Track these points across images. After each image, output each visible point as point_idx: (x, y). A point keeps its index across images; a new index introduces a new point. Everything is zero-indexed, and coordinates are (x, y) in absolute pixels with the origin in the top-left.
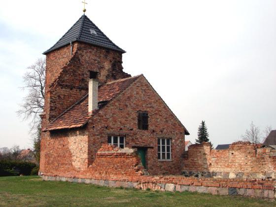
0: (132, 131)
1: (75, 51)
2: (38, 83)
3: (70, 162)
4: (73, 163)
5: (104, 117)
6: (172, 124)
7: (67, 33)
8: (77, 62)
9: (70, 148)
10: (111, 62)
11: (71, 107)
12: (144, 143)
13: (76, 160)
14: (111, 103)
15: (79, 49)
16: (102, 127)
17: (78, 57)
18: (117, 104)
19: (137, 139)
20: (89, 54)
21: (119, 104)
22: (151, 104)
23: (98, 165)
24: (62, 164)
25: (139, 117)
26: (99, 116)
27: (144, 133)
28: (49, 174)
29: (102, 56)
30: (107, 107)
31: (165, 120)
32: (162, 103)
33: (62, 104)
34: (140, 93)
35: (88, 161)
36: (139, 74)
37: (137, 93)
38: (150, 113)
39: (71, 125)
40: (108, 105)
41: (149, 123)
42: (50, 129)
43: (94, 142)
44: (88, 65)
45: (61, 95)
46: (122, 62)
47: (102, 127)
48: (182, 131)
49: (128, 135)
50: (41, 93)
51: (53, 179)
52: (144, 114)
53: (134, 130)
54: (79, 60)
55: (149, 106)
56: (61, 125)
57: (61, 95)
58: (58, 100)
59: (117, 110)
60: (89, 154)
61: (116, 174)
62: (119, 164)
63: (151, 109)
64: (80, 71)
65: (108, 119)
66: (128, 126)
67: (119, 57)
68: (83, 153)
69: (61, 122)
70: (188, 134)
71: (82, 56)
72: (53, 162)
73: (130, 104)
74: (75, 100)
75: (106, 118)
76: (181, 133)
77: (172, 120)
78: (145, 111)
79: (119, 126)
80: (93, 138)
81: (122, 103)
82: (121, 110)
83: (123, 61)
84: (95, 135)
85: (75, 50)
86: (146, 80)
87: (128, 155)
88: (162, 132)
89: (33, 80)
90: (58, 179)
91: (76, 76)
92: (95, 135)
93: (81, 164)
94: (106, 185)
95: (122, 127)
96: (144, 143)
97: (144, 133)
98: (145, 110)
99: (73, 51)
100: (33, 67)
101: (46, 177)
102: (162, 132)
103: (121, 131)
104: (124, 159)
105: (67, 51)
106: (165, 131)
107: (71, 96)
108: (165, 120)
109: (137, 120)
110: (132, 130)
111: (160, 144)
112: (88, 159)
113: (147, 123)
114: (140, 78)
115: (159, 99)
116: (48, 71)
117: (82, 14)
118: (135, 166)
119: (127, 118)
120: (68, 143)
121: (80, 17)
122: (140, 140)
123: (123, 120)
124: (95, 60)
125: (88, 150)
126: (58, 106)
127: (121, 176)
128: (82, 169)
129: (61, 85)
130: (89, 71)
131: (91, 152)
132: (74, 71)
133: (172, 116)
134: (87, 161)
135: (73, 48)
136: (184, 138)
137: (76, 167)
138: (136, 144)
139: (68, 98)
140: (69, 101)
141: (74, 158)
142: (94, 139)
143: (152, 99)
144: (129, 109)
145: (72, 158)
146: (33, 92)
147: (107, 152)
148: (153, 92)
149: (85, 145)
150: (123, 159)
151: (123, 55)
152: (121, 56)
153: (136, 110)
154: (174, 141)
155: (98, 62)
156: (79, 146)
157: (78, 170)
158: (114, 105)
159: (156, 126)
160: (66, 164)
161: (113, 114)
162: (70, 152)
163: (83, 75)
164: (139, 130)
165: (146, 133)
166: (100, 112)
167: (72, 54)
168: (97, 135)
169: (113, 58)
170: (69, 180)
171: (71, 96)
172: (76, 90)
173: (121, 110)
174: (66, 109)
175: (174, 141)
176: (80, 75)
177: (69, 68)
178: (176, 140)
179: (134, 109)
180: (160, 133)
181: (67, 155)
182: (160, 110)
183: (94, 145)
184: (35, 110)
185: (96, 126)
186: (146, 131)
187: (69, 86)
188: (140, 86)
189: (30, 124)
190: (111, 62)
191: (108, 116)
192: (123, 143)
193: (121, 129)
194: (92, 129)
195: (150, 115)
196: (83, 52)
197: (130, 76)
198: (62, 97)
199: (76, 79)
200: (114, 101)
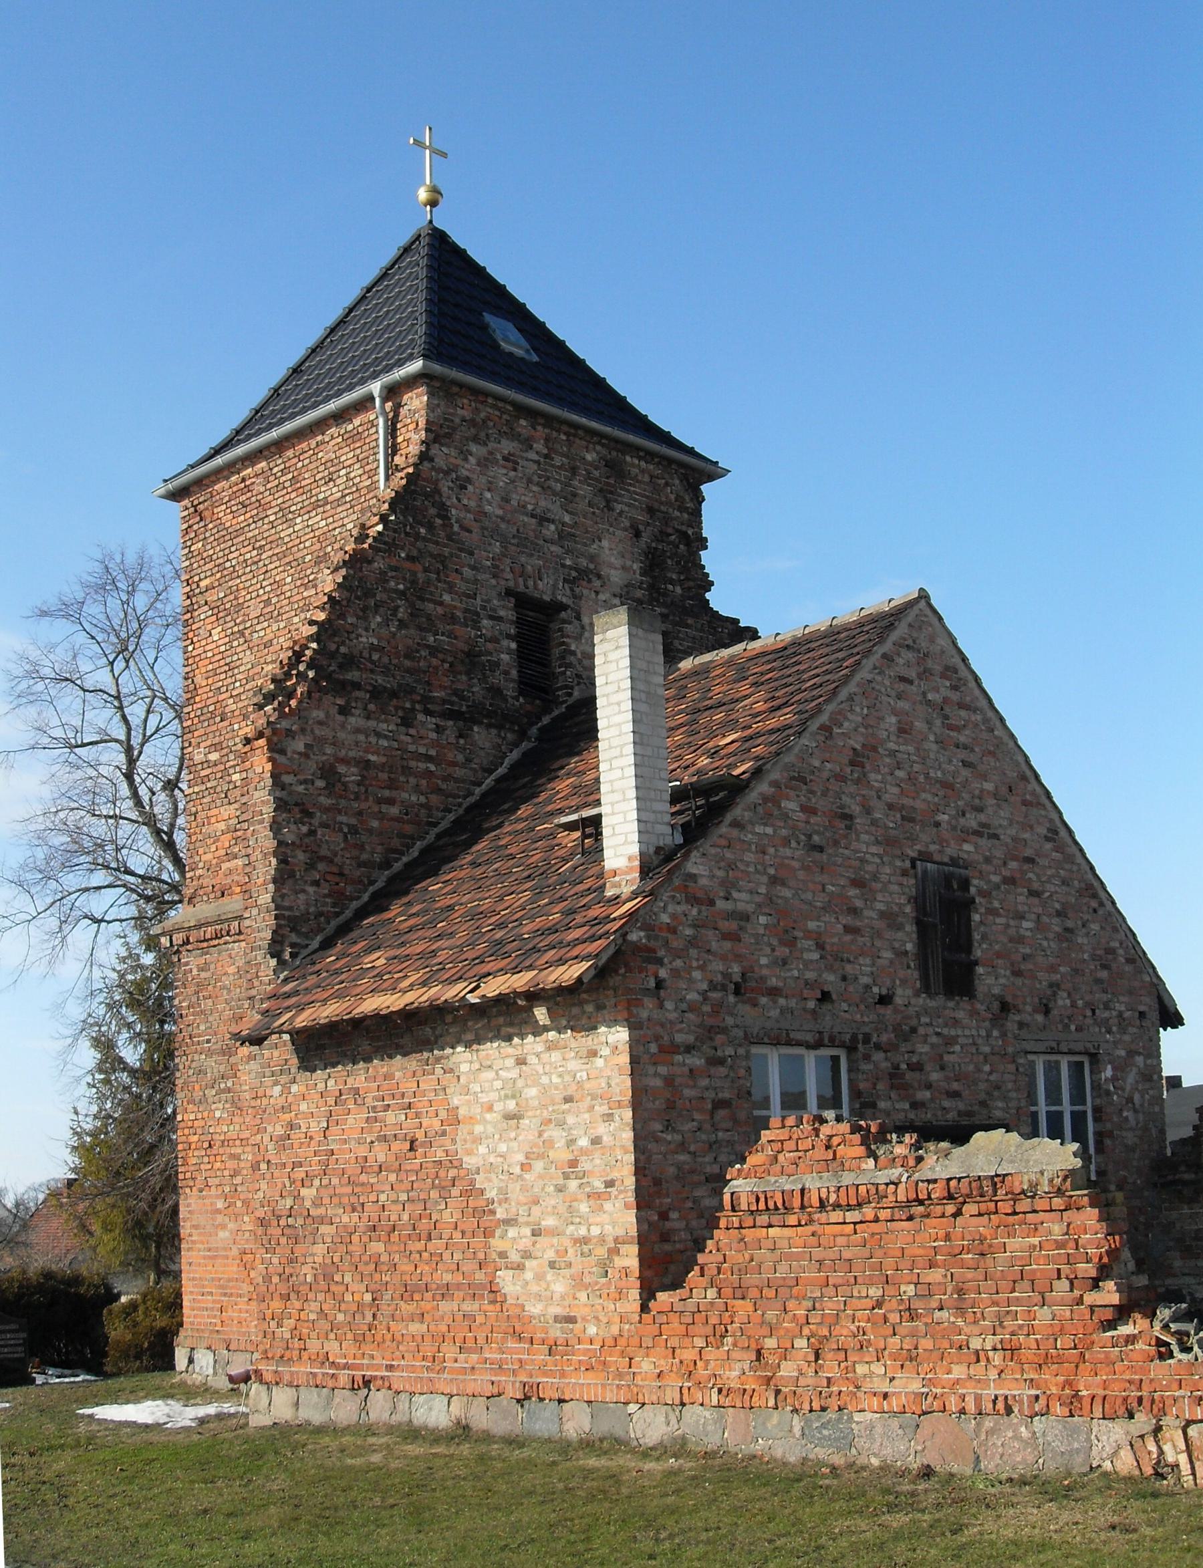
0: (887, 1011)
1: (414, 449)
2: (103, 717)
3: (480, 1276)
4: (507, 1281)
5: (721, 904)
6: (1094, 957)
7: (342, 322)
8: (430, 527)
9: (470, 1162)
10: (637, 534)
11: (414, 852)
12: (956, 1095)
13: (527, 1255)
14: (753, 796)
15: (436, 433)
16: (713, 986)
17: (437, 491)
18: (790, 805)
19: (917, 1067)
20: (502, 476)
21: (808, 810)
22: (980, 810)
23: (741, 1292)
24: (407, 1293)
25: (919, 902)
26: (693, 900)
27: (956, 1022)
28: (303, 1369)
29: (584, 490)
30: (736, 824)
31: (1056, 926)
32: (1040, 805)
33: (354, 830)
34: (919, 725)
35: (645, 1260)
36: (900, 591)
37: (903, 730)
38: (981, 875)
39: (301, 1008)
40: (738, 812)
41: (978, 953)
42: (302, 1021)
43: (671, 1105)
44: (497, 547)
45: (345, 761)
46: (703, 543)
47: (713, 986)
48: (1147, 1003)
49: (867, 1039)
50: (124, 790)
51: (344, 1410)
52: (948, 879)
53: (898, 1000)
54: (445, 516)
55: (971, 821)
56: (382, 982)
57: (345, 761)
58: (325, 801)
59: (794, 854)
60: (643, 1202)
61: (911, 1357)
62: (935, 1275)
63: (983, 842)
64: (451, 588)
65: (745, 917)
66: (862, 969)
67: (682, 509)
68: (594, 1196)
69: (378, 959)
70: (1173, 1019)
71: (462, 484)
72: (327, 1274)
73: (868, 811)
74: (435, 799)
75: (732, 915)
76: (1142, 1015)
77: (1095, 927)
78: (954, 862)
79: (810, 975)
80: (663, 1070)
81: (816, 802)
82: (821, 849)
83: (708, 530)
84: (674, 1049)
85: (412, 440)
86: (950, 634)
87: (1031, 1193)
88: (1047, 1011)
89: (69, 698)
90: (379, 1406)
91: (429, 626)
92: (674, 1049)
93: (578, 1282)
94: (821, 1453)
95: (830, 979)
96: (956, 1095)
97: (956, 1022)
98: (951, 851)
99: (392, 450)
100: (70, 611)
101: (283, 1397)
102: (1047, 1011)
103: (827, 1006)
104: (981, 1226)
105: (347, 456)
106: (1063, 1001)
107: (406, 770)
108: (1056, 926)
109: (911, 928)
110: (885, 1000)
111: (1035, 1104)
112: (642, 1240)
113: (968, 949)
114: (911, 616)
115: (1024, 778)
116: (203, 613)
117: (419, 221)
118: (1095, 1284)
119: (854, 911)
120: (455, 1120)
121: (404, 239)
122: (935, 1076)
123: (832, 926)
124: (543, 520)
125: (639, 1171)
126: (331, 841)
127: (958, 1372)
128: (592, 1330)
129: (342, 687)
130: (509, 593)
131: (657, 1182)
132: (417, 593)
133: (1095, 896)
134: (630, 1258)
135: (392, 431)
136: (1153, 1051)
137: (534, 1309)
138: (915, 1105)
139: (392, 785)
140: (394, 811)
141: (513, 1239)
142: (669, 1081)
143: (984, 777)
144: (865, 845)
145: (497, 1243)
146: (68, 777)
147: (817, 1184)
148: (986, 720)
149: (602, 1129)
150: (971, 1224)
151: (705, 488)
152: (699, 499)
153: (903, 857)
154: (1108, 1072)
155: (562, 536)
156: (549, 1144)
157: (556, 1332)
158: (770, 809)
159: (1017, 973)
160: (446, 1292)
161: (774, 881)
162: (471, 1191)
163: (473, 619)
164: (922, 1000)
165: (960, 1010)
166: (696, 865)
167: (391, 469)
168: (689, 1049)
169: (651, 511)
170: (481, 1418)
171: (406, 770)
172: (439, 729)
173: (821, 849)
174: (386, 864)
175: (1108, 1072)
176: (453, 619)
177: (379, 564)
178: (1120, 1068)
179: (889, 842)
180: (1040, 1018)
181: (447, 1217)
182: (1028, 853)
183: (668, 1126)
184: (98, 904)
185: (675, 973)
186: (965, 1004)
187: (394, 694)
188: (912, 674)
189: (60, 1006)
190: (637, 534)
191: (743, 901)
192: (1084, 1103)
193: (825, 997)
194: (649, 1003)
195: (981, 893)
196: (465, 454)
197: (752, 634)
198: (351, 774)
199: (434, 651)
200: (775, 784)
